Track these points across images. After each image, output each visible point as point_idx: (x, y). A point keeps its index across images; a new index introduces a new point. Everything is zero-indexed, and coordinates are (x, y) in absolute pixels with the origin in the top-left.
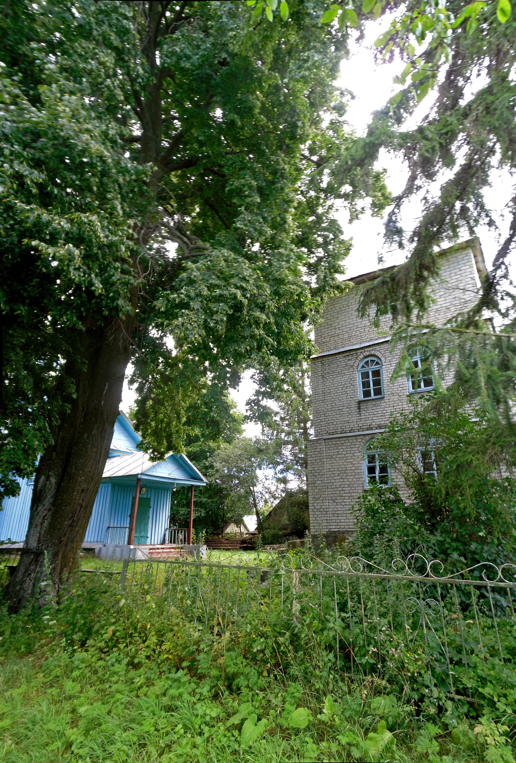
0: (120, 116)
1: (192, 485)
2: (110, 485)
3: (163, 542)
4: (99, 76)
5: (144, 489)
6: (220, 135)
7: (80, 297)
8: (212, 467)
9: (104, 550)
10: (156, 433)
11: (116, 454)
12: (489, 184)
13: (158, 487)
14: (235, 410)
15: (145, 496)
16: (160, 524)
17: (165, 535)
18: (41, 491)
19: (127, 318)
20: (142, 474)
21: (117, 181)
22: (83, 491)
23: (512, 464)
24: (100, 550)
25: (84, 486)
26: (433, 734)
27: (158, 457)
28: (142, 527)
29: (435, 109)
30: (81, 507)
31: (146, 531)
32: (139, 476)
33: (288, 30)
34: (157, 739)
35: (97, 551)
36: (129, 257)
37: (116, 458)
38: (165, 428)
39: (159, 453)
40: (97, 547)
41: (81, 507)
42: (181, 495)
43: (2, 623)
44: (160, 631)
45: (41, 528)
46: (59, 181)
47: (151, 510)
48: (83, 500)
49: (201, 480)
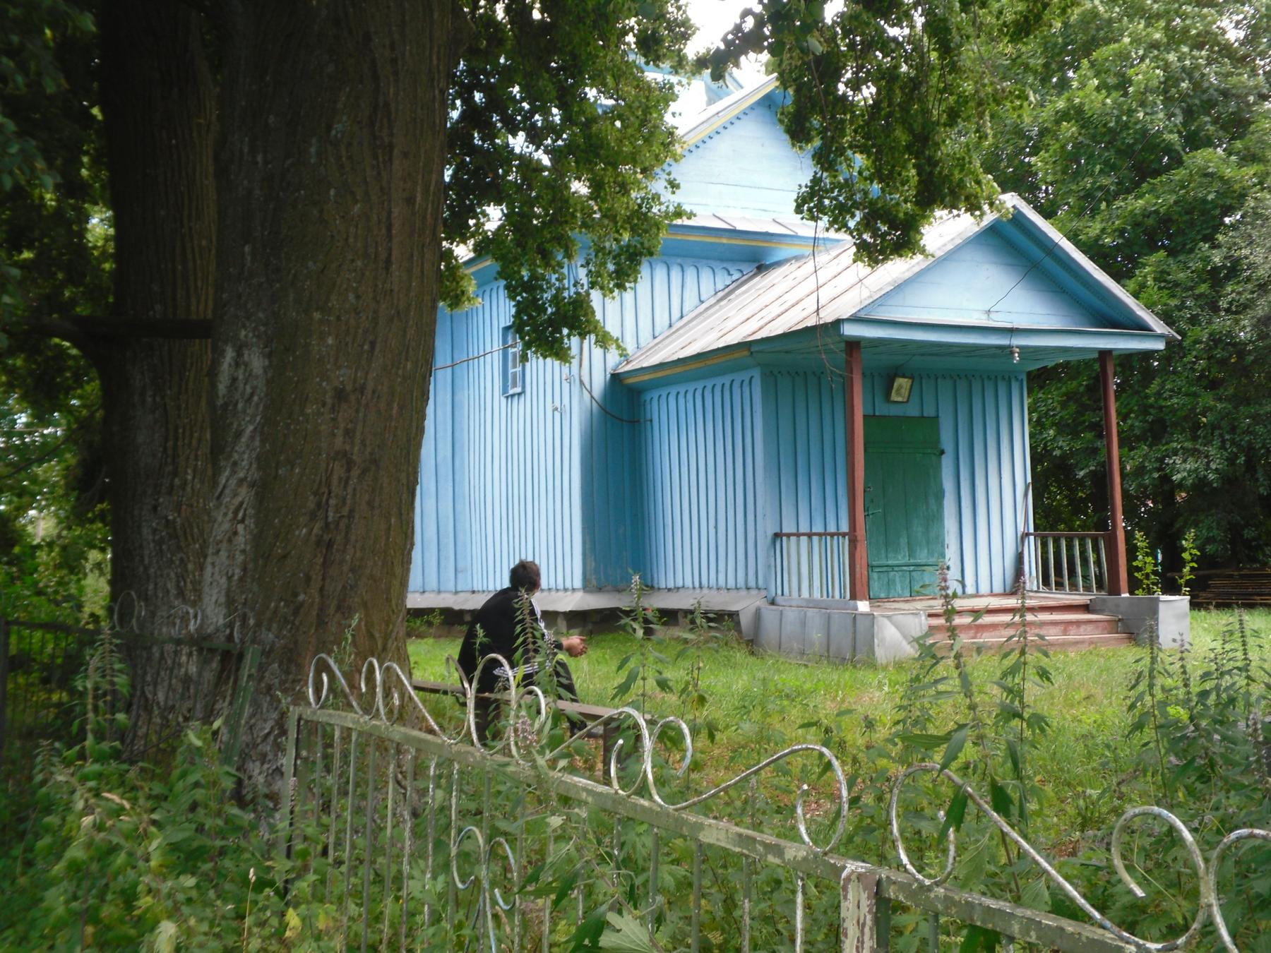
0: (67, 294)
1: (1105, 354)
2: (757, 374)
3: (1016, 585)
4: (1192, 568)
5: (902, 383)
6: (59, 211)
7: (856, 28)
8: (1233, 269)
9: (769, 615)
10: (875, 130)
11: (784, 252)
12: (855, 261)
13: (962, 371)
14: (103, 216)
15: (913, 411)
16: (990, 520)
17: (1019, 559)
18: (225, 406)
19: (550, 109)
20: (855, 319)
21: (423, 792)
22: (340, 395)
23: (422, 950)
24: (758, 615)
25: (343, 375)
26: (708, 742)
27: (889, 235)
28: (918, 529)
29: (599, 316)
30: (350, 464)
31: (937, 544)
32: (850, 330)
33: (607, 69)
34: (1228, 647)
35: (745, 620)
36: (700, 827)
37: (784, 269)
38: (905, 108)
39: (893, 226)
40: (745, 605)
41: (350, 464)
42: (1070, 397)
43: (1268, 68)
44: (1142, 160)
45: (231, 557)
46: (95, 111)
47: (947, 463)
48: (348, 433)
49: (1141, 328)
